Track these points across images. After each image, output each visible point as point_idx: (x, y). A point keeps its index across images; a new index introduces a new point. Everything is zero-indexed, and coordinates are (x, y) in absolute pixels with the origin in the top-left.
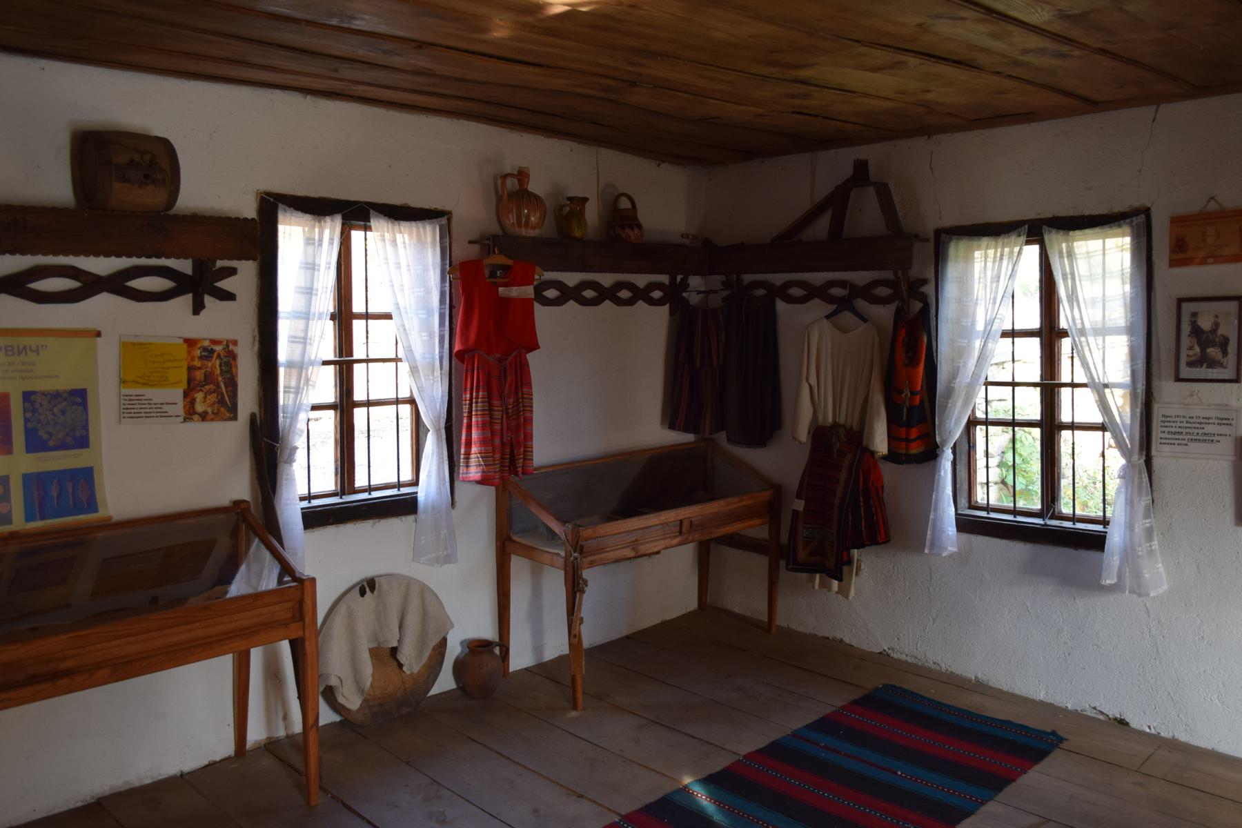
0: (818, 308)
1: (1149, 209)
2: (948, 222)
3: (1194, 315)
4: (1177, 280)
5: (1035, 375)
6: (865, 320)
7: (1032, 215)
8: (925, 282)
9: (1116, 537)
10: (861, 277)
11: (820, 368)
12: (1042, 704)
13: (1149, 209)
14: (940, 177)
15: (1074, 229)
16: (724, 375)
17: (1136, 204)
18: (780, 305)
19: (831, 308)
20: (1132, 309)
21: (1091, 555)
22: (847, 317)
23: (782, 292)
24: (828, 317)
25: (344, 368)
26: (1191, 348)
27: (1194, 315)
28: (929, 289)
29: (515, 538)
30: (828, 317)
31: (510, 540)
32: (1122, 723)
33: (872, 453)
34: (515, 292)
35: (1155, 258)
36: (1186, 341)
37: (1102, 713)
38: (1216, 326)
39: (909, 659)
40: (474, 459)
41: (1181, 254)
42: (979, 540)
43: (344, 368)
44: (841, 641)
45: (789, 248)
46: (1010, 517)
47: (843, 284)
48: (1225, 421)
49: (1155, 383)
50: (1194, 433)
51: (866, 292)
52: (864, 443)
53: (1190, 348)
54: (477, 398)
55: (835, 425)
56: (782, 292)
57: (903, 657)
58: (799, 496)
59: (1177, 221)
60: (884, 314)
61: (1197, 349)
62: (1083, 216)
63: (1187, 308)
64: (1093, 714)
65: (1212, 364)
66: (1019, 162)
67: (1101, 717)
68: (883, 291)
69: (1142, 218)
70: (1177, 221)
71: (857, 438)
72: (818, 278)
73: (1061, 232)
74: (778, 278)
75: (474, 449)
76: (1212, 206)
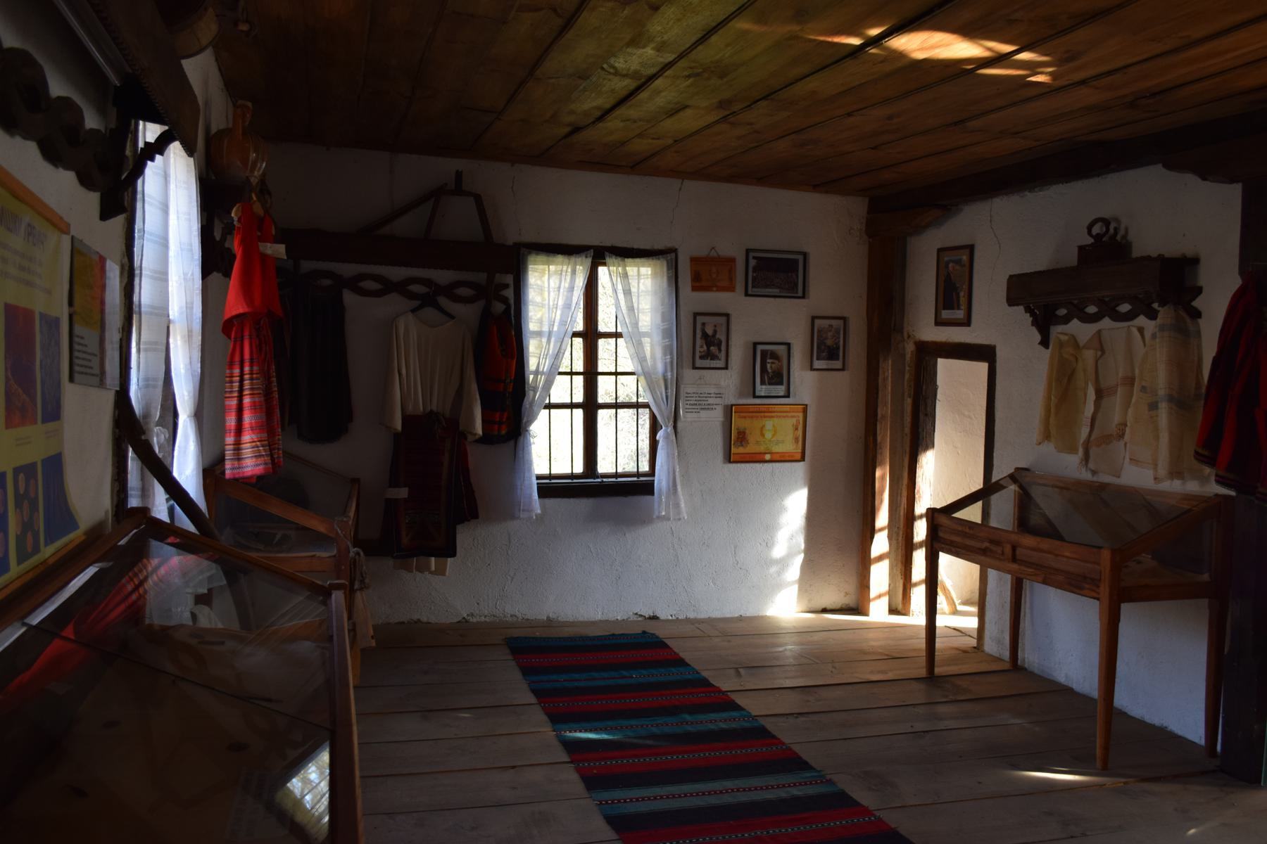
0: (394, 303)
3: (704, 324)
5: (579, 366)
6: (452, 317)
7: (596, 243)
8: (507, 286)
10: (443, 276)
11: (400, 358)
14: (525, 195)
17: (669, 245)
18: (349, 297)
19: (416, 303)
21: (648, 498)
22: (429, 312)
23: (354, 284)
24: (413, 311)
25: (591, 375)
28: (509, 293)
36: (699, 342)
38: (715, 332)
39: (487, 619)
40: (247, 451)
41: (699, 284)
42: (551, 502)
43: (591, 375)
47: (427, 282)
48: (719, 395)
50: (701, 405)
51: (449, 291)
53: (701, 347)
54: (251, 373)
56: (354, 284)
57: (483, 619)
58: (394, 483)
59: (695, 260)
60: (468, 313)
63: (700, 320)
64: (635, 618)
65: (714, 357)
66: (587, 199)
68: (464, 292)
69: (673, 255)
70: (695, 260)
71: (454, 428)
72: (397, 273)
74: (348, 269)
75: (247, 438)
76: (713, 254)
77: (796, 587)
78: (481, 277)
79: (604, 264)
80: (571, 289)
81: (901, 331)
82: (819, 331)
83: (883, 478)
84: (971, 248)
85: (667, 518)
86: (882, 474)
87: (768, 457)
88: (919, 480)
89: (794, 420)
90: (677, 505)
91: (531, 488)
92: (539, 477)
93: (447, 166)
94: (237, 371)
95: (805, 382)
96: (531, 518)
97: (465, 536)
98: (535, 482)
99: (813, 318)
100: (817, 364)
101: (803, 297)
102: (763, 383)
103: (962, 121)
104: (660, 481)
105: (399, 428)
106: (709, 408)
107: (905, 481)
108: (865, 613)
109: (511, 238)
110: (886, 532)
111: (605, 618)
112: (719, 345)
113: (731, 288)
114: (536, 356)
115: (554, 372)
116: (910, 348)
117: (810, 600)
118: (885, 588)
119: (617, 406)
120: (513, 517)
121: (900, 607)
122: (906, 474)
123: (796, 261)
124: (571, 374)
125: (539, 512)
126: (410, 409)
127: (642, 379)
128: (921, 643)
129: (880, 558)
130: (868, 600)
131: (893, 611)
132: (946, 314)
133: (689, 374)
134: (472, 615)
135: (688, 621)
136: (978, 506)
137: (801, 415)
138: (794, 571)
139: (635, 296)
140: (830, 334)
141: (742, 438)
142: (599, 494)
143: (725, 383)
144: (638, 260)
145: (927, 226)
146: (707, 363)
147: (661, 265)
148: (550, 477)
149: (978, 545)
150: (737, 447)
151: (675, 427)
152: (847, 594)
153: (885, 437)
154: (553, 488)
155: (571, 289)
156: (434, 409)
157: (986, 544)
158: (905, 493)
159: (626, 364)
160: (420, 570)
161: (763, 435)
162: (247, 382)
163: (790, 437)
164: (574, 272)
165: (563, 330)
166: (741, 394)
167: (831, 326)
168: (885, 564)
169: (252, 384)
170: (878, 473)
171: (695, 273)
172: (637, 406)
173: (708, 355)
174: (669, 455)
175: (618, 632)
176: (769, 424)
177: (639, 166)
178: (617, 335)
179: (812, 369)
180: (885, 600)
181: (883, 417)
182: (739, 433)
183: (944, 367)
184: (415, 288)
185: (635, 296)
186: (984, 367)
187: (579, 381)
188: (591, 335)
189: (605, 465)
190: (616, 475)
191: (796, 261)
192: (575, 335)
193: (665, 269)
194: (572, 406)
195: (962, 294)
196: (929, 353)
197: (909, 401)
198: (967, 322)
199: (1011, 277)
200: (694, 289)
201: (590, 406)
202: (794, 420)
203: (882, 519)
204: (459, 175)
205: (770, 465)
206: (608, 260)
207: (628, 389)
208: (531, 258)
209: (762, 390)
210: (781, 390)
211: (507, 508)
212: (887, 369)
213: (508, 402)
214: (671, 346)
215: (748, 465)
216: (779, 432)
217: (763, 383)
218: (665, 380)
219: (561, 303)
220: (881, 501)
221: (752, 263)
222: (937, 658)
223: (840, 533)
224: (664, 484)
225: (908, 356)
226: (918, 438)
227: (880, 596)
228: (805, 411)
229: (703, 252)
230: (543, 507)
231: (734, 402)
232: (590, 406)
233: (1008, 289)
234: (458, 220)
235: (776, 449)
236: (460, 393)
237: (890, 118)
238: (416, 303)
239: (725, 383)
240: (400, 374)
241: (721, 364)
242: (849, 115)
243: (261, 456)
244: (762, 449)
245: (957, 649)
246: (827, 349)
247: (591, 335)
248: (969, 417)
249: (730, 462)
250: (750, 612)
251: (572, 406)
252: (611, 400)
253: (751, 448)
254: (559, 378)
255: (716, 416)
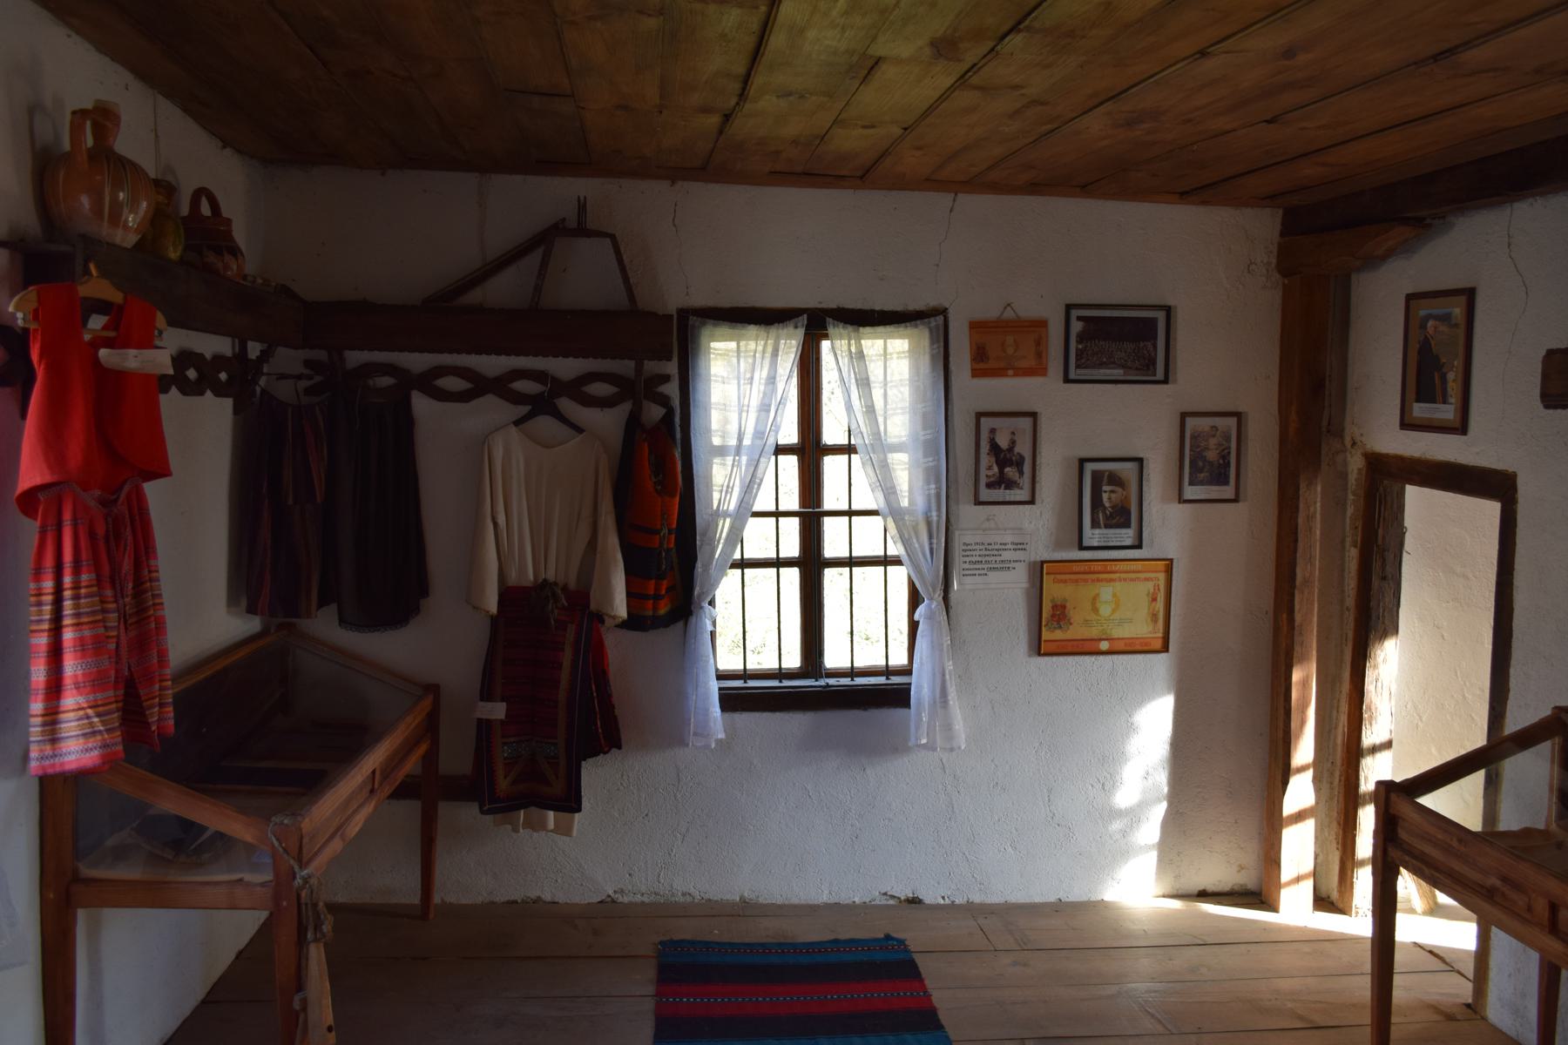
0: (492, 410)
1: (945, 310)
2: (700, 300)
4: (979, 392)
5: (791, 501)
6: (580, 430)
7: (812, 303)
8: (666, 379)
9: (921, 686)
10: (566, 367)
11: (500, 496)
12: (828, 906)
13: (945, 310)
14: (690, 235)
15: (864, 325)
16: (335, 518)
18: (421, 404)
19: (524, 409)
20: (926, 422)
21: (899, 713)
22: (545, 425)
23: (426, 382)
24: (517, 423)
25: (811, 519)
26: (990, 468)
27: (993, 431)
28: (672, 389)
29: (86, 871)
30: (517, 423)
31: (77, 879)
32: (914, 901)
33: (599, 618)
34: (132, 360)
35: (953, 367)
37: (893, 897)
38: (1013, 442)
39: (646, 899)
40: (70, 724)
41: (984, 364)
42: (744, 719)
43: (811, 519)
44: (538, 900)
45: (448, 316)
46: (881, 680)
47: (539, 376)
48: (1020, 546)
49: (953, 507)
50: (991, 560)
51: (575, 389)
52: (593, 607)
54: (76, 586)
55: (543, 586)
56: (426, 382)
57: (638, 898)
58: (487, 695)
59: (976, 326)
60: (608, 422)
61: (996, 469)
62: (873, 311)
65: (1011, 485)
66: (795, 235)
67: (892, 902)
68: (600, 389)
69: (940, 319)
70: (976, 326)
71: (580, 604)
72: (492, 364)
73: (850, 328)
74: (417, 362)
75: (70, 701)
76: (1009, 314)
77: (1154, 855)
78: (625, 367)
79: (826, 337)
80: (772, 380)
81: (1340, 434)
82: (1193, 437)
83: (1305, 683)
84: (1470, 294)
85: (930, 747)
86: (1305, 678)
87: (1104, 646)
88: (1369, 686)
89: (1150, 585)
90: (948, 727)
91: (707, 696)
92: (721, 676)
93: (555, 195)
94: (48, 585)
95: (1168, 523)
96: (707, 746)
97: (595, 775)
98: (714, 686)
99: (1184, 416)
100: (1191, 492)
101: (1166, 381)
102: (1095, 524)
103: (1451, 51)
104: (920, 687)
105: (493, 607)
106: (1005, 567)
107: (1346, 686)
108: (1273, 908)
109: (674, 299)
110: (1310, 774)
111: (832, 901)
112: (1019, 464)
113: (1039, 370)
114: (720, 482)
115: (747, 511)
116: (1356, 464)
117: (1177, 877)
118: (1308, 866)
119: (851, 562)
120: (683, 743)
121: (1335, 895)
122: (1346, 675)
123: (1153, 321)
124: (777, 514)
125: (721, 736)
126: (513, 578)
127: (890, 520)
128: (1362, 988)
129: (1299, 817)
130: (1279, 886)
131: (1322, 902)
132: (1420, 410)
133: (969, 514)
134: (622, 891)
135: (972, 910)
136: (1475, 782)
137: (1162, 577)
138: (1150, 830)
139: (882, 383)
140: (1213, 442)
141: (1060, 614)
142: (822, 701)
143: (1033, 526)
144: (880, 329)
145: (1384, 258)
146: (1000, 494)
147: (922, 334)
148: (745, 675)
149: (1475, 876)
150: (1052, 630)
151: (946, 599)
152: (1241, 868)
153: (1310, 615)
154: (748, 696)
155: (772, 380)
156: (551, 576)
157: (1493, 881)
158: (1344, 707)
159: (865, 498)
160: (529, 825)
161: (1095, 610)
162: (68, 604)
163: (1143, 612)
164: (775, 353)
165: (759, 443)
166: (1059, 545)
167: (1214, 428)
168: (1309, 826)
169: (76, 606)
170: (1297, 676)
171: (975, 352)
172: (885, 561)
173: (1002, 482)
174: (935, 647)
175: (845, 934)
176: (1106, 592)
177: (865, 174)
178: (849, 450)
179: (1181, 500)
180: (1308, 885)
181: (1306, 581)
182: (1055, 607)
183: (1416, 499)
184: (522, 386)
185: (882, 383)
186: (1491, 510)
187: (791, 527)
188: (810, 451)
189: (835, 657)
190: (852, 672)
191: (1153, 321)
192: (780, 450)
193: (926, 342)
194: (778, 563)
195: (1451, 376)
196: (1389, 476)
197: (1353, 554)
198: (1461, 428)
199: (1551, 354)
200: (976, 373)
201: (812, 563)
202: (1150, 585)
203: (1304, 751)
204: (582, 207)
205: (1109, 658)
206: (831, 330)
207: (870, 537)
208: (706, 332)
209: (1093, 536)
210: (1126, 536)
211: (673, 729)
212: (1314, 499)
213: (670, 562)
214: (937, 468)
215: (1070, 659)
216: (1123, 604)
217: (1095, 524)
218: (929, 524)
219: (755, 402)
220: (1303, 722)
221: (1077, 327)
222: (1399, 957)
223: (1231, 766)
224: (926, 691)
225: (1353, 477)
226: (1370, 619)
227: (1298, 879)
228: (1169, 566)
229: (991, 312)
230: (730, 729)
231: (1046, 556)
232: (812, 563)
233: (1546, 377)
234: (584, 279)
235: (1117, 632)
236: (592, 545)
237: (1289, 53)
238: (524, 409)
239: (1033, 526)
240: (495, 524)
241: (1022, 494)
242: (1203, 53)
243: (94, 733)
244: (1094, 632)
245: (1434, 1008)
246: (1208, 465)
247: (810, 451)
248: (1465, 577)
249: (1040, 654)
250: (1076, 893)
251: (778, 563)
252: (843, 553)
253: (1075, 632)
254: (752, 521)
255: (1015, 583)
